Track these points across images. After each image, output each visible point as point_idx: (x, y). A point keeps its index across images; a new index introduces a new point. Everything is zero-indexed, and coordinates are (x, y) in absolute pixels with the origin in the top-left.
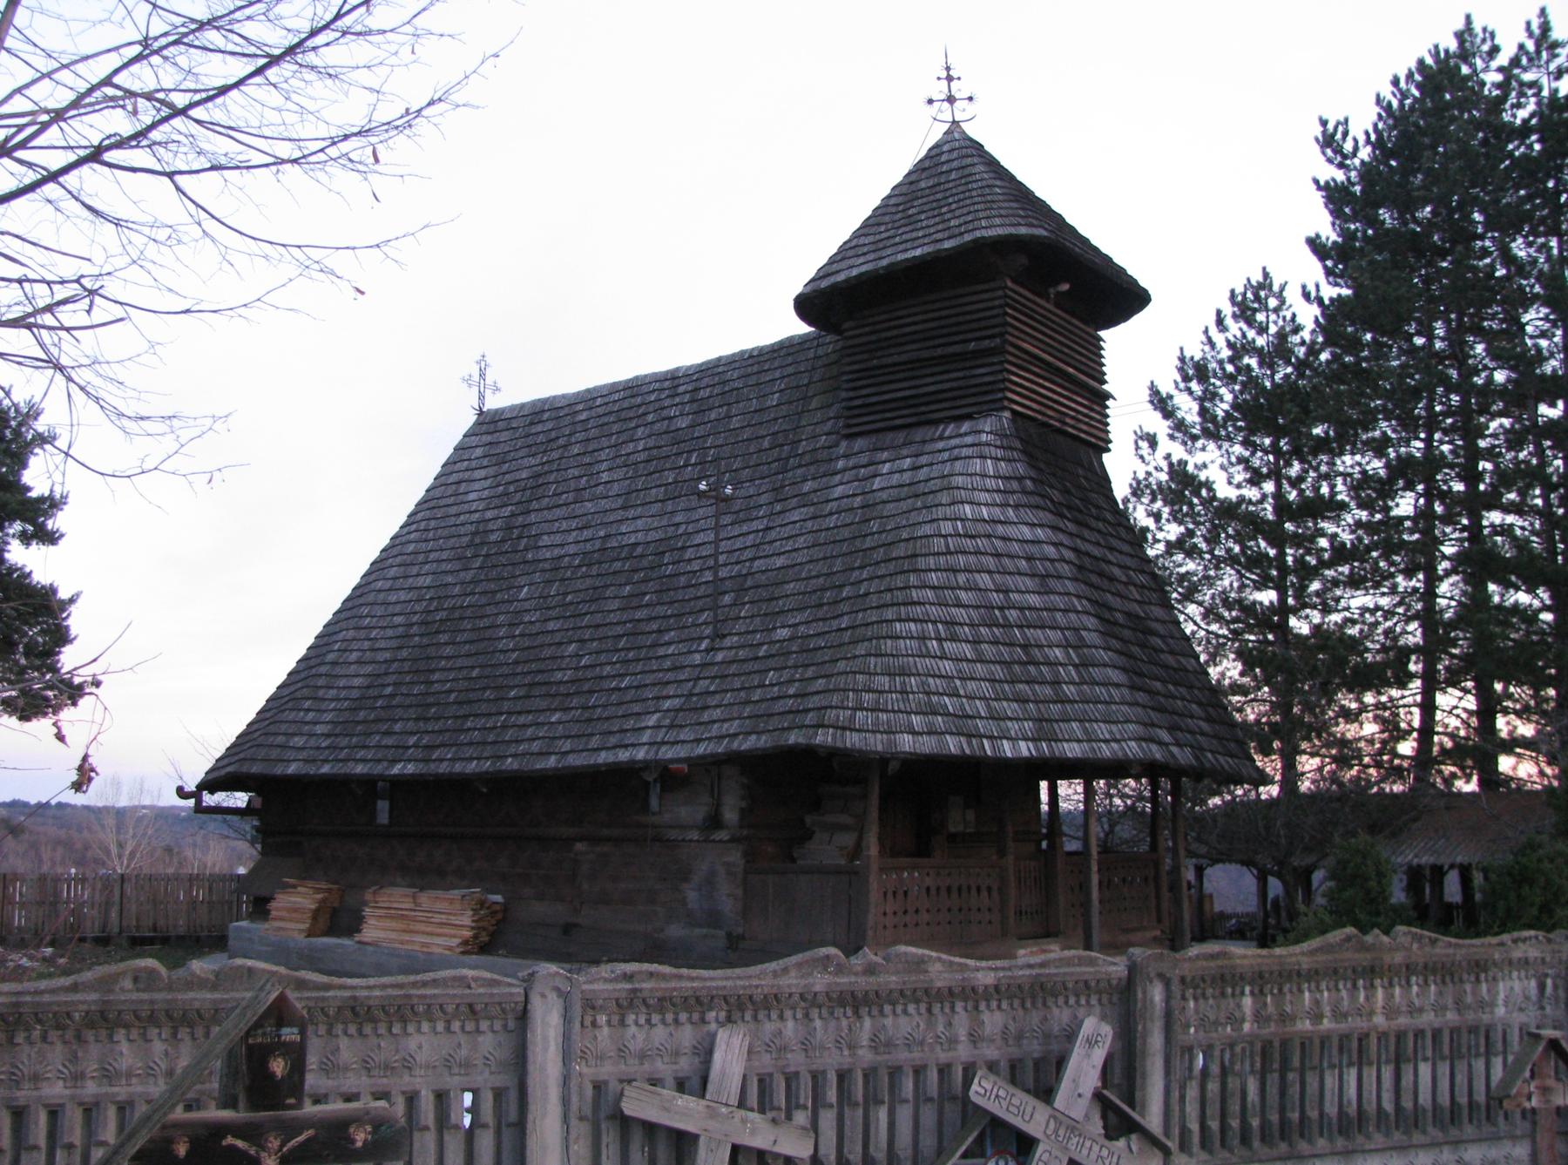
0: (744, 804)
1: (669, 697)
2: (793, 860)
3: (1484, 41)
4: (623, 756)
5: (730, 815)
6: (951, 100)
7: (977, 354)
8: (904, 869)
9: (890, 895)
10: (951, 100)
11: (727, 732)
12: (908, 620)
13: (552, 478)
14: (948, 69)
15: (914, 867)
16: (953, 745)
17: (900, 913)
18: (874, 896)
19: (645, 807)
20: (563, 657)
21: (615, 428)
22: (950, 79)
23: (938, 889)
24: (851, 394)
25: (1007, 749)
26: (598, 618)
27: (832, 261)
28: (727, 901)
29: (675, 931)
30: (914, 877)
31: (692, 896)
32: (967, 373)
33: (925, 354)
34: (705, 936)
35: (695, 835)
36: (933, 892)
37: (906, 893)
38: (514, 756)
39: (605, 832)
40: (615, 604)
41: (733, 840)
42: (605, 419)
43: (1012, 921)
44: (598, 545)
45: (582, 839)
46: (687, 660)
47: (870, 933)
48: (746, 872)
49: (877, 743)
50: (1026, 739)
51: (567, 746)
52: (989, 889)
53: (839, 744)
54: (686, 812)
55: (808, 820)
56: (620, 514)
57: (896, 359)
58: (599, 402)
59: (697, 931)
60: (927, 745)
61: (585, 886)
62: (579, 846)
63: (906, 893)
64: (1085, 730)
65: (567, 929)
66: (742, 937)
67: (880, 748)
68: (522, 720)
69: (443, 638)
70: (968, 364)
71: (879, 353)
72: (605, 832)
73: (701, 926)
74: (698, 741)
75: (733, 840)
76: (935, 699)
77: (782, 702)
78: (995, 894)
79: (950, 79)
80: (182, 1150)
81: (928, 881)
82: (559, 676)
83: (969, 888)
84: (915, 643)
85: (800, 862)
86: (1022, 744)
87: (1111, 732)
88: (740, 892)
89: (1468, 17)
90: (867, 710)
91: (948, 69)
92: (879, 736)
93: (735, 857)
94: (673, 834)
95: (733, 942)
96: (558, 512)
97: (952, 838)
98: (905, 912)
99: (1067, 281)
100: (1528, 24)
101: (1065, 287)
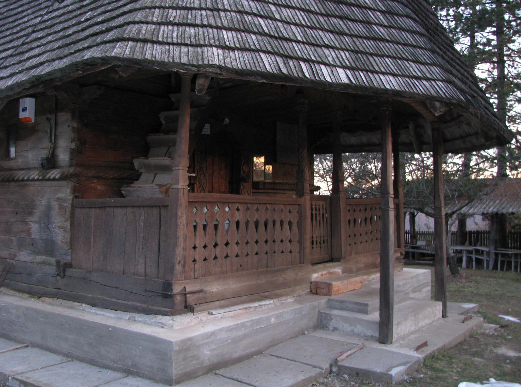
8: (213, 203)
9: (200, 228)
15: (225, 203)
16: (268, 63)
17: (210, 247)
18: (183, 229)
23: (247, 223)
25: (325, 74)
30: (227, 213)
35: (35, 175)
36: (242, 225)
37: (216, 227)
41: (63, 178)
43: (308, 250)
47: (178, 268)
48: (73, 207)
49: (182, 56)
50: (343, 67)
52: (290, 223)
55: (136, 163)
60: (238, 61)
63: (216, 227)
64: (399, 67)
66: (69, 265)
67: (184, 60)
75: (63, 178)
76: (248, 19)
78: (295, 227)
80: (431, 153)
81: (238, 216)
83: (274, 222)
86: (340, 71)
87: (421, 71)
88: (68, 224)
90: (173, 24)
92: (184, 49)
93: (65, 192)
94: (21, 175)
95: (63, 268)
97: (256, 186)
98: (216, 245)
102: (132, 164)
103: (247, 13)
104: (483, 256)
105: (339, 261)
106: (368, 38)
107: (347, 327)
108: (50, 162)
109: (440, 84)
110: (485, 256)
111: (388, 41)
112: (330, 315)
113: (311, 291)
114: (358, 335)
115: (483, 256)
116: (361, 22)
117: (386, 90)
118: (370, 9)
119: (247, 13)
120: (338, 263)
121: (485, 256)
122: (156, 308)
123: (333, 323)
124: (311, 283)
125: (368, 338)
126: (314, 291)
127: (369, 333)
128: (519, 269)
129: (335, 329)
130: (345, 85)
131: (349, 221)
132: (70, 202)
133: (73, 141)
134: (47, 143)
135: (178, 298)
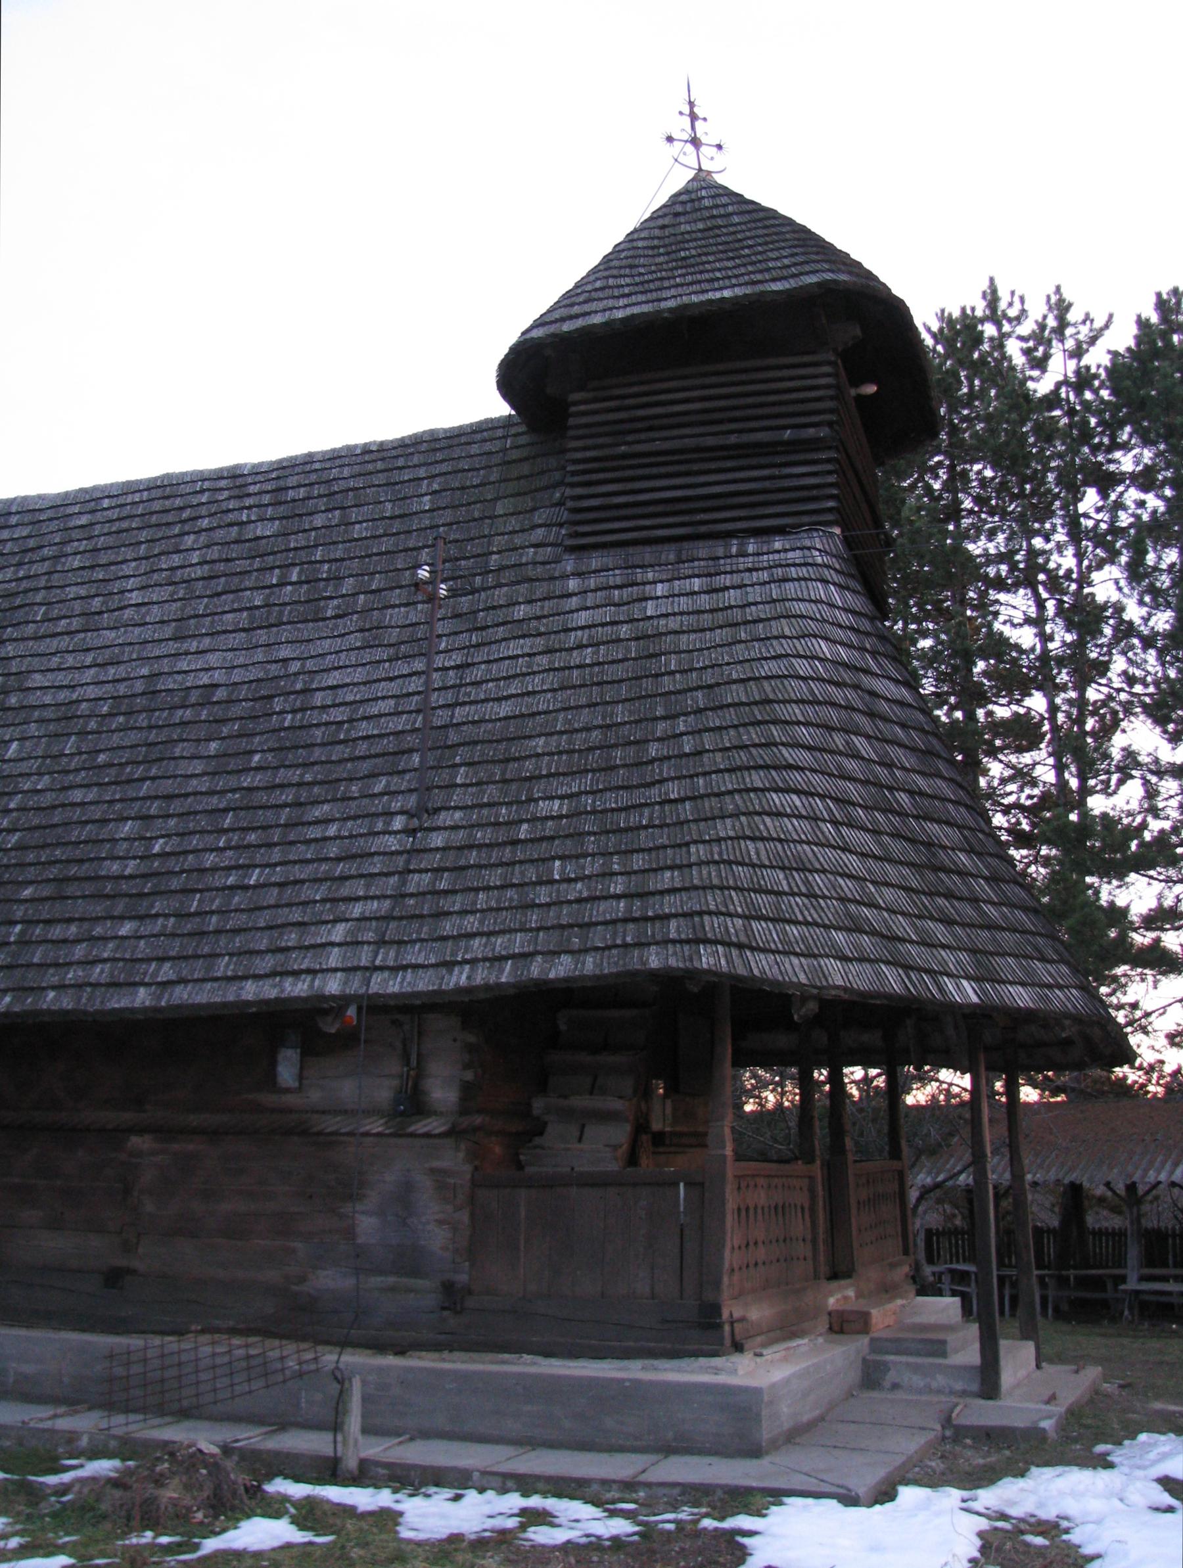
0: (469, 1076)
1: (357, 899)
2: (520, 1166)
3: (1011, 304)
4: (299, 988)
5: (442, 1092)
6: (695, 142)
7: (794, 446)
10: (695, 142)
11: (484, 957)
12: (788, 790)
13: (39, 598)
14: (691, 104)
16: (893, 980)
19: (270, 1081)
20: (114, 841)
21: (144, 535)
22: (693, 117)
23: (756, 1208)
24: (579, 491)
26: (168, 786)
27: (568, 299)
28: (436, 1231)
29: (330, 1280)
31: (367, 1225)
32: (776, 472)
33: (711, 441)
34: (393, 1289)
38: (60, 987)
39: (194, 1120)
40: (198, 767)
42: (125, 525)
44: (139, 686)
45: (141, 1131)
46: (377, 844)
48: (475, 1184)
51: (167, 972)
53: (741, 971)
54: (355, 1090)
56: (172, 647)
57: (658, 445)
58: (106, 503)
59: (376, 1281)
61: (149, 1207)
62: (135, 1141)
65: (114, 1278)
68: (57, 932)
69: (295, 667)
70: (778, 460)
71: (629, 438)
72: (194, 1120)
73: (382, 1272)
74: (449, 965)
77: (603, 905)
79: (693, 117)
82: (115, 868)
84: (805, 825)
85: (530, 1170)
88: (464, 1217)
89: (992, 280)
91: (691, 104)
94: (331, 1124)
95: (453, 1296)
96: (54, 644)
99: (872, 382)
100: (1048, 297)
101: (871, 389)
102: (529, 1105)
103: (849, 900)
104: (969, 1285)
105: (849, 1276)
106: (981, 927)
107: (918, 1381)
108: (412, 1102)
109: (1074, 991)
110: (973, 1284)
111: (1003, 929)
112: (885, 1363)
113: (831, 1329)
114: (939, 1391)
115: (969, 1285)
116: (967, 899)
117: (1020, 1008)
118: (972, 875)
119: (849, 900)
120: (848, 1281)
121: (973, 1284)
122: (690, 1347)
123: (891, 1377)
124: (830, 1314)
125: (964, 1393)
126: (836, 1328)
127: (959, 1386)
128: (1050, 1311)
129: (895, 1386)
130: (976, 1005)
131: (739, 1209)
132: (469, 1176)
133: (466, 1066)
134: (394, 1066)
135: (727, 1328)
